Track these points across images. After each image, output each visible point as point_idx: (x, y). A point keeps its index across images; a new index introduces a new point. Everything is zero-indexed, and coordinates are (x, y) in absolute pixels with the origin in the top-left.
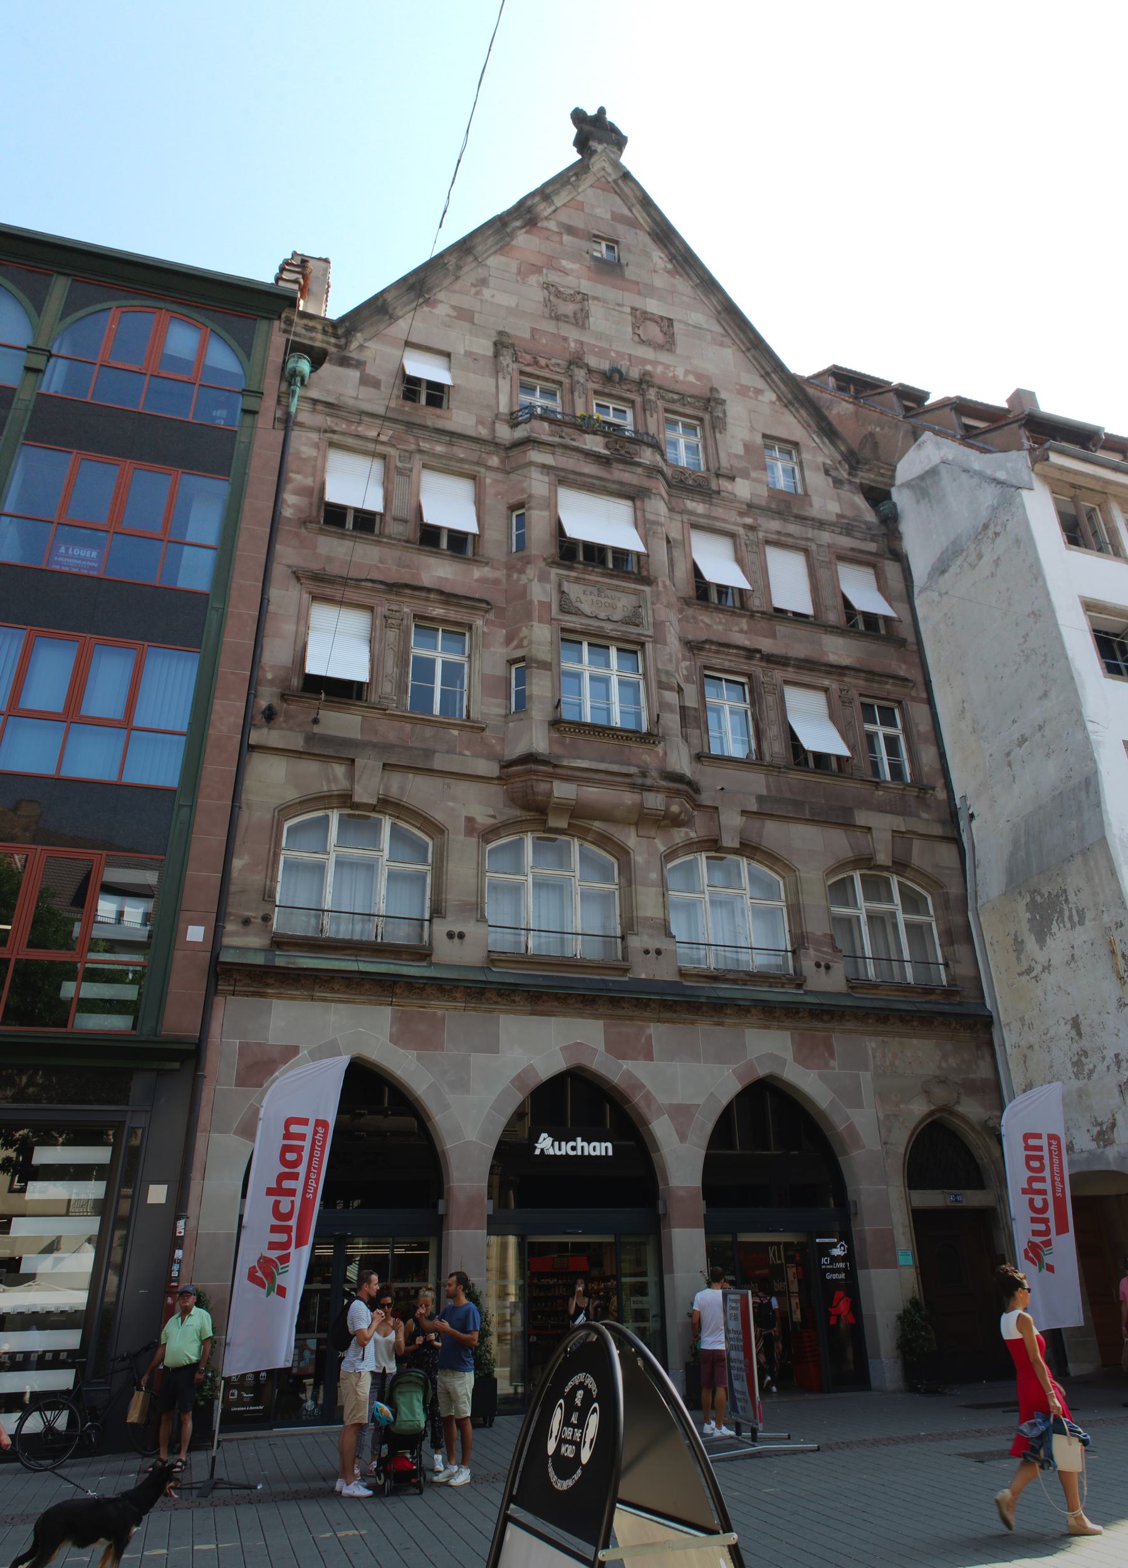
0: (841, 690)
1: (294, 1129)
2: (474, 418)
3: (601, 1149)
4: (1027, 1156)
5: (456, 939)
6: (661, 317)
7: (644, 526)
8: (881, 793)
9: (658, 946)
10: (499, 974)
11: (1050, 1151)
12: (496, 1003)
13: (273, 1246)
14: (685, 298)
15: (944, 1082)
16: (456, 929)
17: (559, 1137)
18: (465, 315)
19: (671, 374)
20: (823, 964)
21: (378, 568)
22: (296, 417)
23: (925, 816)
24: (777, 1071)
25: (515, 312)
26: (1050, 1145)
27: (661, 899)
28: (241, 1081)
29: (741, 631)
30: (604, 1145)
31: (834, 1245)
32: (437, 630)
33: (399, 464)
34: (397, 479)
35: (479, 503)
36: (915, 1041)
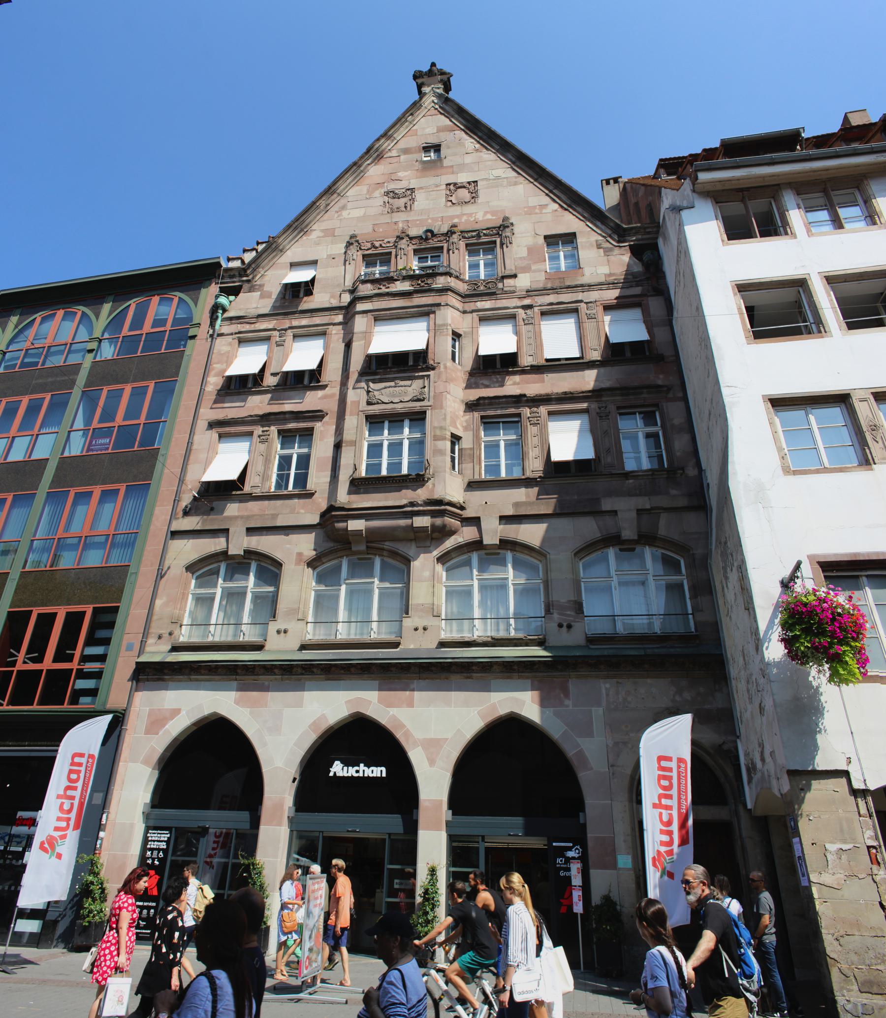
0: (599, 408)
1: (77, 760)
2: (329, 295)
3: (378, 772)
4: (659, 775)
5: (282, 634)
6: (469, 183)
7: (435, 331)
8: (631, 481)
9: (425, 623)
10: (597, 650)
12: (302, 674)
13: (57, 829)
14: (490, 163)
16: (283, 628)
17: (347, 763)
18: (330, 233)
20: (565, 624)
22: (220, 330)
23: (674, 492)
24: (517, 710)
26: (679, 767)
27: (431, 590)
28: (147, 732)
29: (515, 384)
30: (379, 769)
31: (570, 849)
33: (588, 312)
34: (276, 349)
36: (649, 681)
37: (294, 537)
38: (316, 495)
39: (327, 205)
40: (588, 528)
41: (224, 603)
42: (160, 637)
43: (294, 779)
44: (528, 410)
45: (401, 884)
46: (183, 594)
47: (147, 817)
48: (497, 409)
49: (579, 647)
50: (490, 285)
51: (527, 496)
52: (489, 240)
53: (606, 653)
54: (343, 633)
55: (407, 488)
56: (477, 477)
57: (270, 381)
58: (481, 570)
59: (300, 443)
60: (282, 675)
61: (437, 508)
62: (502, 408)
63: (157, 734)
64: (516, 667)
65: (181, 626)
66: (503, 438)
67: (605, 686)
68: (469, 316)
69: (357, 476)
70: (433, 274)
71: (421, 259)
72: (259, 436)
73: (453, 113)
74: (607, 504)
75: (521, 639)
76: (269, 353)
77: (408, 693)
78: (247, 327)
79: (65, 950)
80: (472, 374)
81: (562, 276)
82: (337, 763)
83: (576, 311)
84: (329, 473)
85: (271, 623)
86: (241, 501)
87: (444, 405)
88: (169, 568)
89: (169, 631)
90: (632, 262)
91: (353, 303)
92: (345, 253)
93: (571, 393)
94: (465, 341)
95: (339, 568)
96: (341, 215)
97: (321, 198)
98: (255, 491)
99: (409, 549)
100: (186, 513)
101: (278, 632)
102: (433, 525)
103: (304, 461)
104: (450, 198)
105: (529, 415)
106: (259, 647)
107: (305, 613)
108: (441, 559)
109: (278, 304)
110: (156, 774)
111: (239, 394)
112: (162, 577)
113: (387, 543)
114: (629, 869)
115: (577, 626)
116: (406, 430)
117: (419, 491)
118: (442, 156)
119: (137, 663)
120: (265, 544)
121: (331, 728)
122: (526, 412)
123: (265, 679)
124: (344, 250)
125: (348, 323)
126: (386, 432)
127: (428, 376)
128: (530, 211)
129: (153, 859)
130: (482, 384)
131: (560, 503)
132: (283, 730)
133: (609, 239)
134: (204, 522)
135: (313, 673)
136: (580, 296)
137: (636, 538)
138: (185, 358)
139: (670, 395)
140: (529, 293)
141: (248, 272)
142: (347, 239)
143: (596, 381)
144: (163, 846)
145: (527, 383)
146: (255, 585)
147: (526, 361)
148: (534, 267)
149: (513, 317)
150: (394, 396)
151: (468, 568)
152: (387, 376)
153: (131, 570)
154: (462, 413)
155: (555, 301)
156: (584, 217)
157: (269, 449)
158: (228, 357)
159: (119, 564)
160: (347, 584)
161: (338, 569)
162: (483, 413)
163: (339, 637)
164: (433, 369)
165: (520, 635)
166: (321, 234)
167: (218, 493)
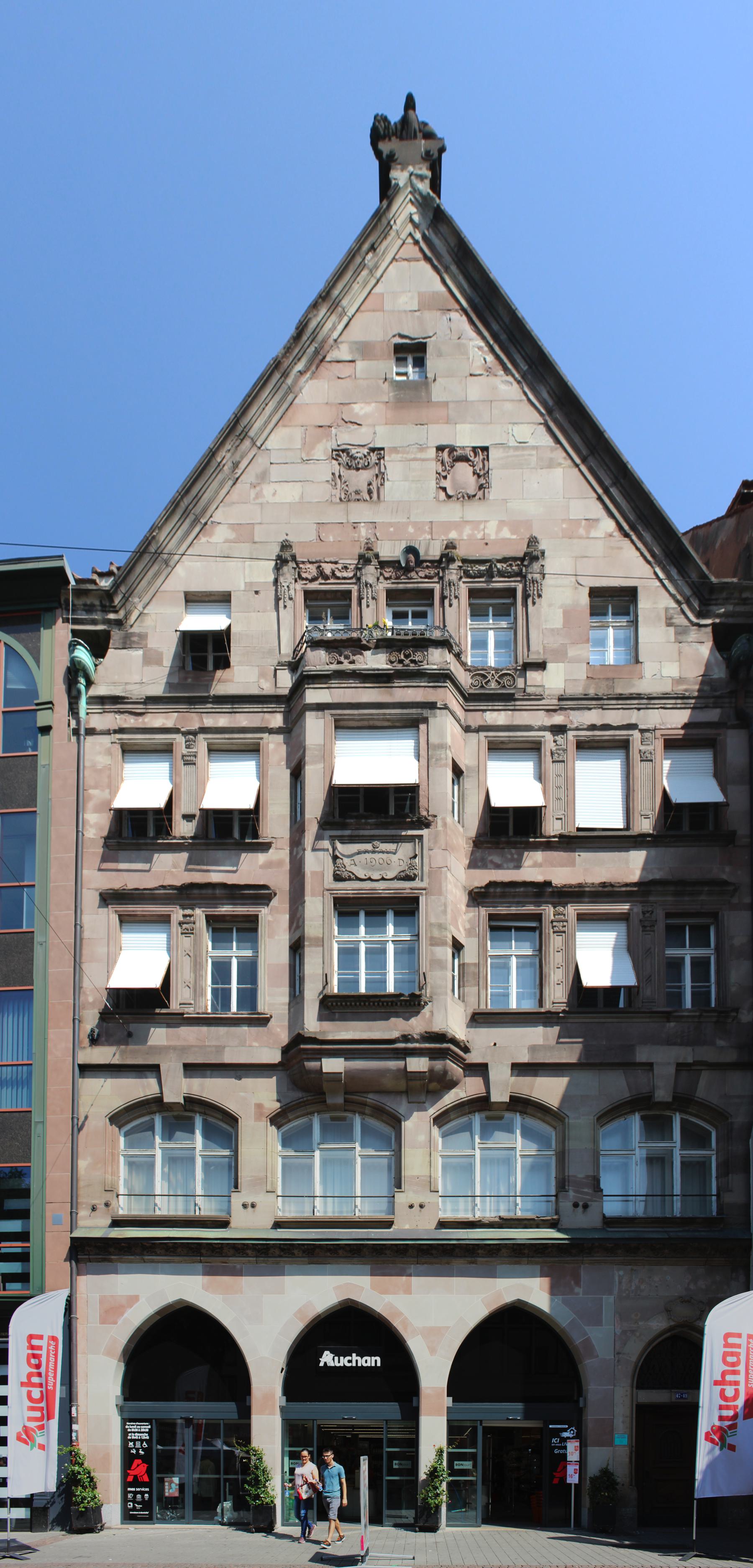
0: (644, 913)
2: (256, 671)
3: (372, 1361)
6: (474, 449)
7: (426, 755)
8: (672, 1024)
11: (48, 1350)
12: (281, 1256)
14: (508, 406)
15: (689, 1301)
16: (249, 1201)
17: (338, 1353)
19: (479, 536)
20: (581, 1204)
21: (172, 873)
22: (87, 722)
23: (721, 1043)
25: (300, 506)
27: (428, 1158)
28: (103, 1321)
29: (536, 865)
30: (374, 1358)
31: (565, 1430)
32: (232, 929)
33: (643, 748)
34: (185, 770)
35: (545, 792)
36: (665, 1268)
37: (249, 1082)
38: (272, 1020)
39: (236, 465)
40: (618, 1085)
41: (166, 1170)
42: (94, 1209)
43: (283, 1369)
44: (552, 909)
45: (400, 1464)
46: (113, 1154)
47: (121, 1409)
48: (510, 904)
49: (595, 1229)
50: (505, 681)
51: (546, 1038)
52: (505, 585)
53: (627, 1235)
54: (323, 1209)
55: (397, 1015)
56: (483, 1007)
57: (183, 829)
58: (485, 1135)
59: (238, 941)
60: (257, 1257)
61: (438, 1046)
62: (518, 903)
63: (115, 1323)
64: (526, 1251)
65: (118, 1196)
66: (517, 950)
67: (619, 1275)
68: (473, 736)
69: (328, 991)
70: (422, 643)
71: (397, 616)
72: (181, 924)
73: (447, 258)
74: (642, 1055)
75: (533, 1219)
76: (173, 776)
77: (404, 1278)
78: (131, 722)
79: (64, 1533)
80: (478, 843)
81: (610, 675)
82: (327, 1353)
83: (624, 745)
84: (286, 989)
85: (233, 1194)
86: (169, 1025)
87: (444, 889)
88: (86, 1118)
89: (104, 1201)
90: (713, 660)
91: (298, 688)
92: (276, 581)
93: (612, 885)
94: (468, 782)
95: (309, 1129)
96: (258, 495)
97: (223, 443)
98: (186, 1010)
99: (400, 1106)
100: (94, 1041)
101: (245, 1206)
102: (431, 1071)
103: (249, 971)
104: (444, 483)
105: (552, 917)
106: (224, 1224)
107: (279, 1180)
108: (440, 1120)
109: (175, 680)
110: (122, 1367)
111: (138, 847)
112: (80, 1130)
113: (371, 1096)
114: (625, 1446)
115: (593, 1206)
116: (390, 928)
117: (413, 1021)
118: (430, 375)
119: (71, 1238)
120: (212, 1089)
121: (319, 1316)
122: (549, 911)
123: (236, 1261)
124: (271, 578)
125: (292, 730)
126: (362, 929)
127: (420, 837)
128: (572, 530)
129: (137, 1450)
130: (491, 861)
131: (587, 1050)
132: (265, 1318)
133: (685, 607)
134: (123, 1053)
135: (293, 1255)
136: (633, 717)
137: (670, 1100)
138: (41, 771)
139: (735, 900)
140: (565, 702)
141: (117, 600)
142: (276, 550)
143: (644, 869)
144: (146, 1437)
145: (553, 865)
146: (205, 1147)
147: (552, 827)
148: (572, 652)
149: (535, 748)
150: (372, 868)
151: (468, 1134)
152: (362, 832)
153: (35, 1118)
154: (463, 907)
155: (599, 723)
156: (653, 555)
157: (197, 944)
158: (109, 777)
159: (14, 1109)
160: (321, 1150)
161: (308, 1130)
162: (492, 910)
163: (317, 1214)
164: (427, 825)
165: (529, 1215)
166: (232, 535)
167: (135, 1009)
